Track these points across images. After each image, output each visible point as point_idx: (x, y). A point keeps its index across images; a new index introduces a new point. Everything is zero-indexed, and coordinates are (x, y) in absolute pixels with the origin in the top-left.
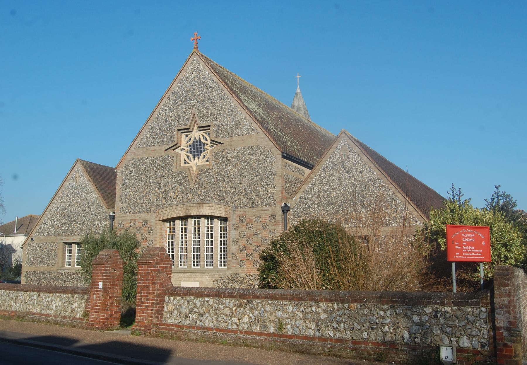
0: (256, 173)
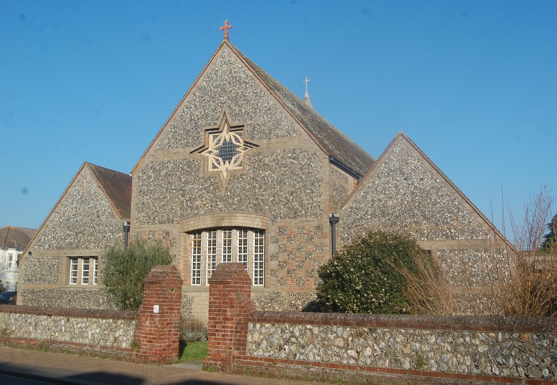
0: (299, 180)
